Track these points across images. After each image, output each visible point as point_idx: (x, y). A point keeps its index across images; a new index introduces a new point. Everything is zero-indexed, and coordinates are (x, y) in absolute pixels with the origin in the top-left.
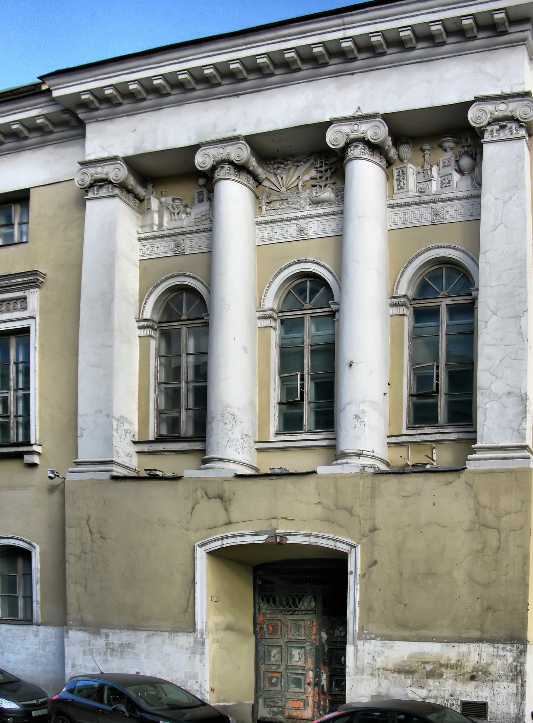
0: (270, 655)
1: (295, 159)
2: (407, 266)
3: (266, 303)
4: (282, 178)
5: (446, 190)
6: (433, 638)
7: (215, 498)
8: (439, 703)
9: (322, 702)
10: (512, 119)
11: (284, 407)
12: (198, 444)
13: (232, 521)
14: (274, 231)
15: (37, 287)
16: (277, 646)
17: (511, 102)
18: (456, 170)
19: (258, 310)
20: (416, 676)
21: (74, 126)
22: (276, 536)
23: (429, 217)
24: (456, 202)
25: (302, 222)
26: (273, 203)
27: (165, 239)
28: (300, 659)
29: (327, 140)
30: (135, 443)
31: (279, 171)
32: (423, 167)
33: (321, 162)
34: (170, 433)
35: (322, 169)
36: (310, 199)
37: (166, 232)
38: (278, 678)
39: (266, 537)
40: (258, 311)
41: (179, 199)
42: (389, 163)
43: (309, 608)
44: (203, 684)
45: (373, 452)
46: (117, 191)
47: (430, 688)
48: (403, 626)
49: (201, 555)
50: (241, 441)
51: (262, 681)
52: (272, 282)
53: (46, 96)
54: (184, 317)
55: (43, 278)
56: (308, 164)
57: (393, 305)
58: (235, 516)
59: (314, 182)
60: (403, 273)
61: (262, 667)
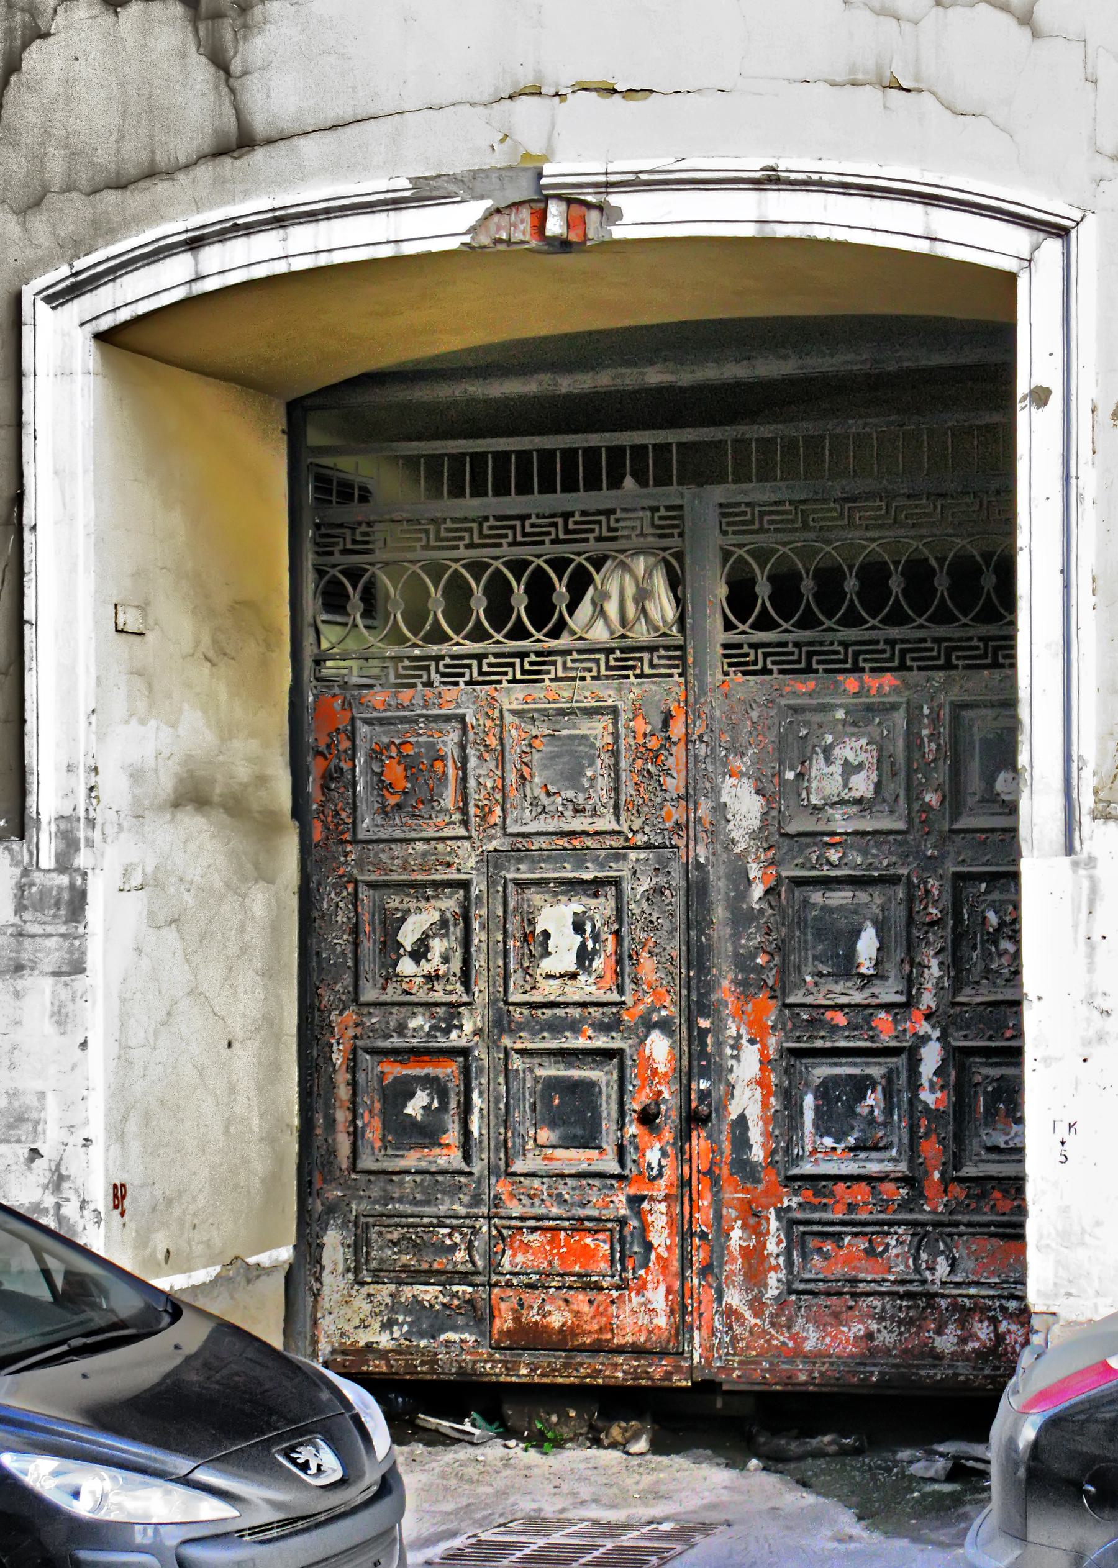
0: (390, 947)
9: (736, 1234)
13: (260, 124)
16: (435, 884)
28: (584, 957)
38: (439, 1088)
43: (641, 633)
44: (71, 1168)
51: (342, 1116)
58: (274, 98)
61: (343, 1023)
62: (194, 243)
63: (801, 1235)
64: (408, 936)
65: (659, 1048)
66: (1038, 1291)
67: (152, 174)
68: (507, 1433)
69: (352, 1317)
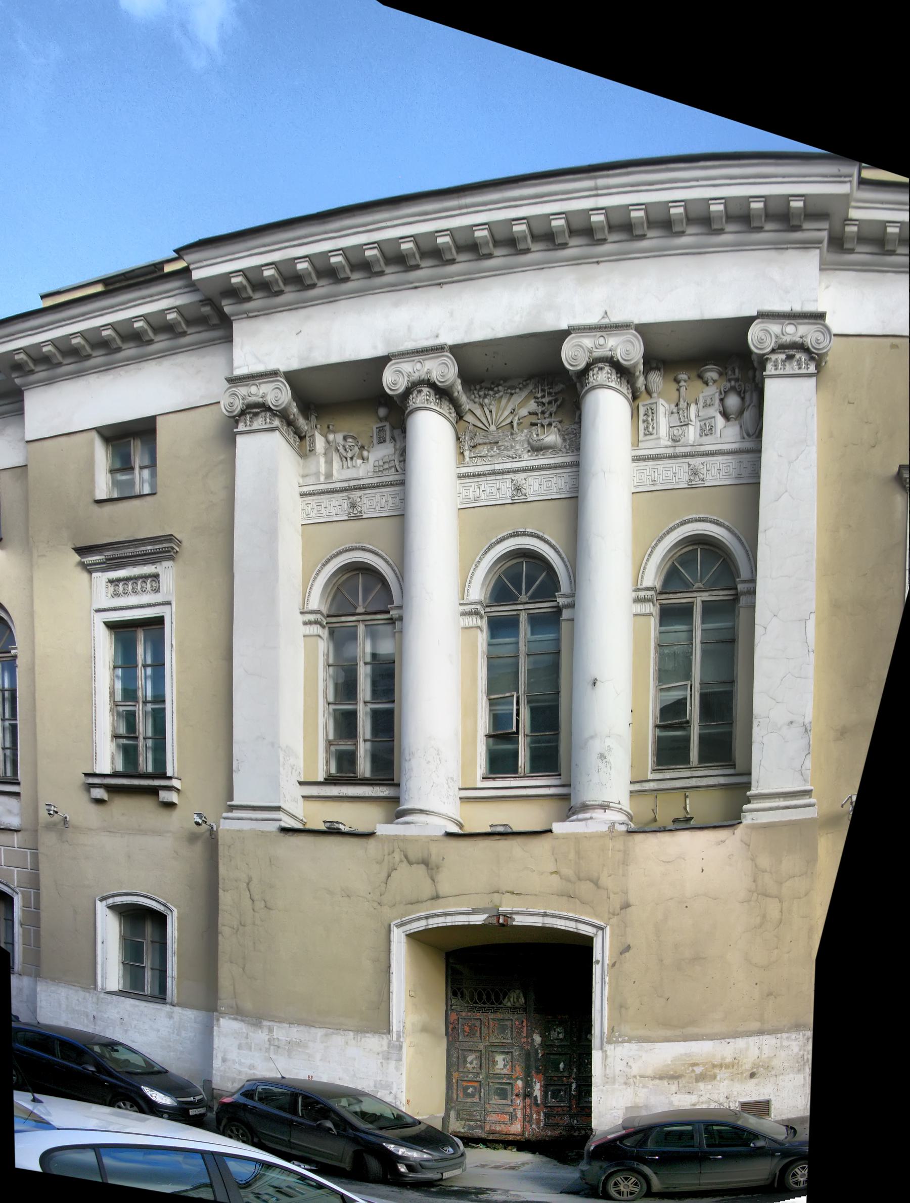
0: (465, 1061)
1: (508, 384)
2: (656, 545)
3: (471, 593)
4: (491, 412)
5: (705, 440)
6: (703, 1035)
7: (418, 863)
8: (712, 1107)
10: (802, 347)
11: (491, 740)
12: (384, 788)
13: (441, 894)
14: (482, 488)
15: (171, 558)
17: (801, 324)
18: (720, 412)
19: (462, 602)
20: (683, 1081)
21: (214, 325)
22: (498, 916)
23: (685, 477)
24: (720, 458)
25: (519, 477)
26: (480, 448)
27: (335, 495)
28: (505, 1066)
30: (301, 783)
31: (486, 401)
32: (677, 405)
33: (543, 390)
34: (344, 771)
35: (546, 400)
36: (529, 443)
37: (338, 485)
39: (485, 916)
40: (461, 604)
41: (354, 438)
42: (635, 397)
43: (517, 1005)
45: (619, 803)
46: (277, 422)
47: (700, 1093)
48: (666, 1024)
49: (398, 938)
50: (446, 786)
51: (455, 1091)
52: (479, 562)
53: (181, 279)
54: (360, 610)
55: (178, 546)
56: (524, 394)
57: (637, 600)
58: (445, 887)
59: (534, 419)
60: (650, 555)
61: (455, 1075)
62: (427, 917)
63: (547, 1116)
64: (469, 1059)
65: (520, 1083)
66: (594, 1125)
67: (418, 902)
68: (488, 1147)
69: (456, 1126)
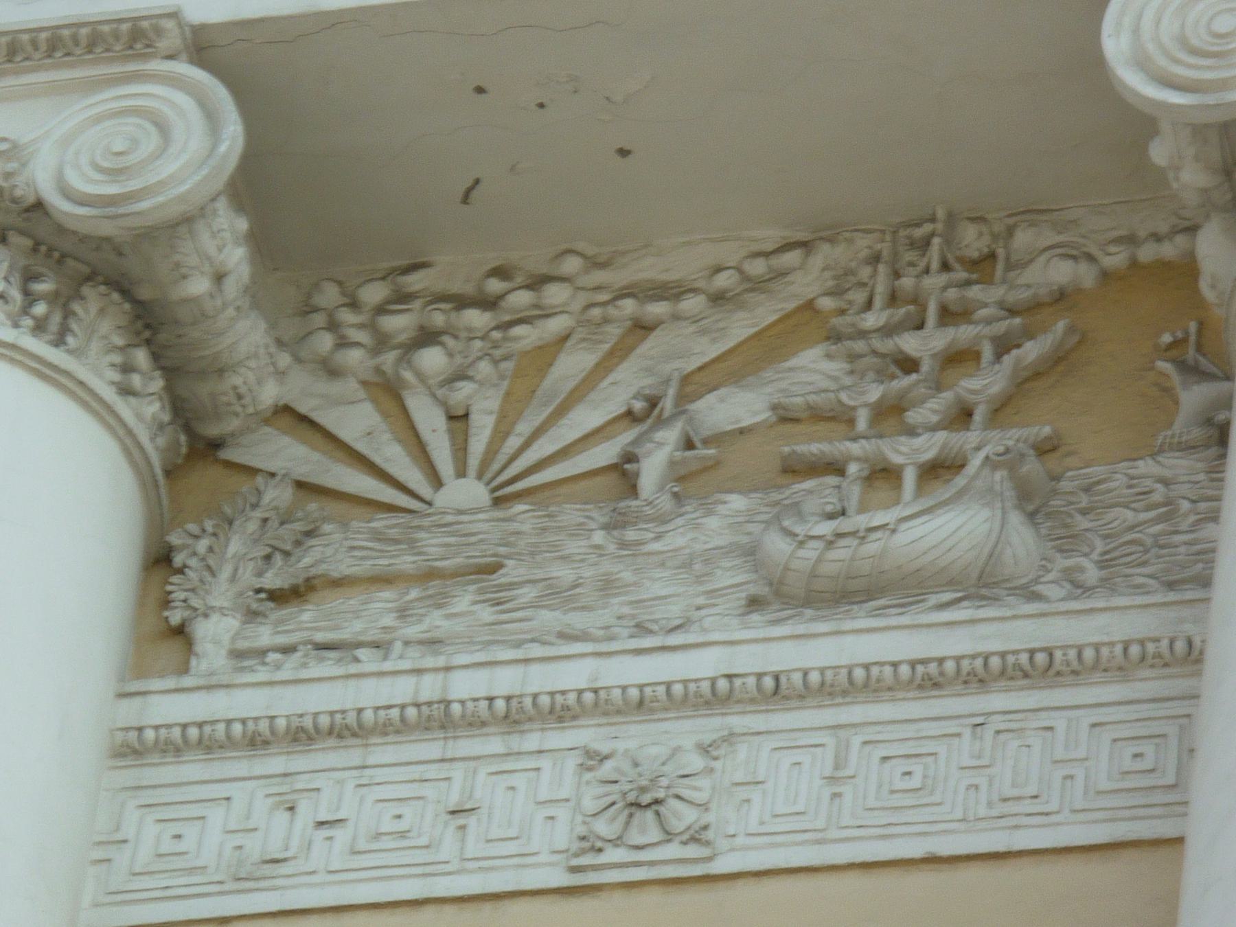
4: (459, 419)
26: (335, 602)
29: (1115, 45)
